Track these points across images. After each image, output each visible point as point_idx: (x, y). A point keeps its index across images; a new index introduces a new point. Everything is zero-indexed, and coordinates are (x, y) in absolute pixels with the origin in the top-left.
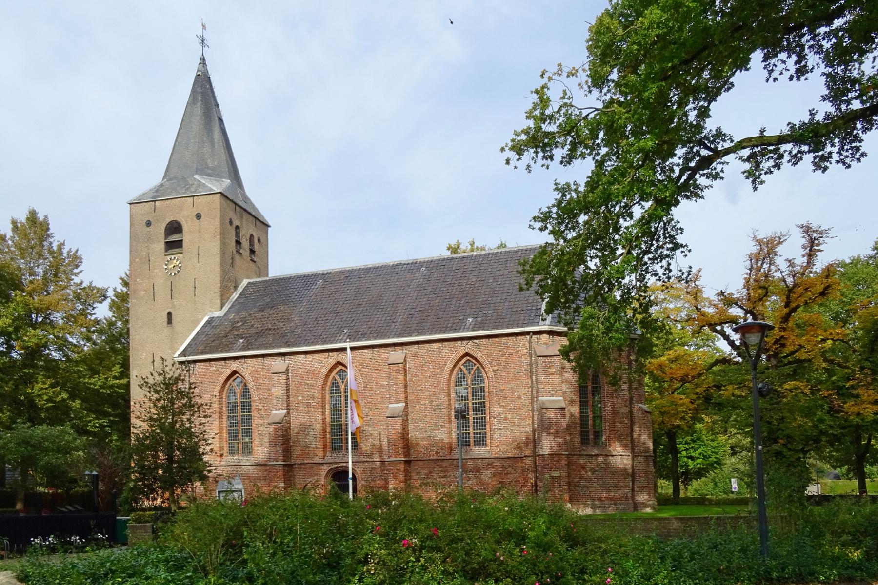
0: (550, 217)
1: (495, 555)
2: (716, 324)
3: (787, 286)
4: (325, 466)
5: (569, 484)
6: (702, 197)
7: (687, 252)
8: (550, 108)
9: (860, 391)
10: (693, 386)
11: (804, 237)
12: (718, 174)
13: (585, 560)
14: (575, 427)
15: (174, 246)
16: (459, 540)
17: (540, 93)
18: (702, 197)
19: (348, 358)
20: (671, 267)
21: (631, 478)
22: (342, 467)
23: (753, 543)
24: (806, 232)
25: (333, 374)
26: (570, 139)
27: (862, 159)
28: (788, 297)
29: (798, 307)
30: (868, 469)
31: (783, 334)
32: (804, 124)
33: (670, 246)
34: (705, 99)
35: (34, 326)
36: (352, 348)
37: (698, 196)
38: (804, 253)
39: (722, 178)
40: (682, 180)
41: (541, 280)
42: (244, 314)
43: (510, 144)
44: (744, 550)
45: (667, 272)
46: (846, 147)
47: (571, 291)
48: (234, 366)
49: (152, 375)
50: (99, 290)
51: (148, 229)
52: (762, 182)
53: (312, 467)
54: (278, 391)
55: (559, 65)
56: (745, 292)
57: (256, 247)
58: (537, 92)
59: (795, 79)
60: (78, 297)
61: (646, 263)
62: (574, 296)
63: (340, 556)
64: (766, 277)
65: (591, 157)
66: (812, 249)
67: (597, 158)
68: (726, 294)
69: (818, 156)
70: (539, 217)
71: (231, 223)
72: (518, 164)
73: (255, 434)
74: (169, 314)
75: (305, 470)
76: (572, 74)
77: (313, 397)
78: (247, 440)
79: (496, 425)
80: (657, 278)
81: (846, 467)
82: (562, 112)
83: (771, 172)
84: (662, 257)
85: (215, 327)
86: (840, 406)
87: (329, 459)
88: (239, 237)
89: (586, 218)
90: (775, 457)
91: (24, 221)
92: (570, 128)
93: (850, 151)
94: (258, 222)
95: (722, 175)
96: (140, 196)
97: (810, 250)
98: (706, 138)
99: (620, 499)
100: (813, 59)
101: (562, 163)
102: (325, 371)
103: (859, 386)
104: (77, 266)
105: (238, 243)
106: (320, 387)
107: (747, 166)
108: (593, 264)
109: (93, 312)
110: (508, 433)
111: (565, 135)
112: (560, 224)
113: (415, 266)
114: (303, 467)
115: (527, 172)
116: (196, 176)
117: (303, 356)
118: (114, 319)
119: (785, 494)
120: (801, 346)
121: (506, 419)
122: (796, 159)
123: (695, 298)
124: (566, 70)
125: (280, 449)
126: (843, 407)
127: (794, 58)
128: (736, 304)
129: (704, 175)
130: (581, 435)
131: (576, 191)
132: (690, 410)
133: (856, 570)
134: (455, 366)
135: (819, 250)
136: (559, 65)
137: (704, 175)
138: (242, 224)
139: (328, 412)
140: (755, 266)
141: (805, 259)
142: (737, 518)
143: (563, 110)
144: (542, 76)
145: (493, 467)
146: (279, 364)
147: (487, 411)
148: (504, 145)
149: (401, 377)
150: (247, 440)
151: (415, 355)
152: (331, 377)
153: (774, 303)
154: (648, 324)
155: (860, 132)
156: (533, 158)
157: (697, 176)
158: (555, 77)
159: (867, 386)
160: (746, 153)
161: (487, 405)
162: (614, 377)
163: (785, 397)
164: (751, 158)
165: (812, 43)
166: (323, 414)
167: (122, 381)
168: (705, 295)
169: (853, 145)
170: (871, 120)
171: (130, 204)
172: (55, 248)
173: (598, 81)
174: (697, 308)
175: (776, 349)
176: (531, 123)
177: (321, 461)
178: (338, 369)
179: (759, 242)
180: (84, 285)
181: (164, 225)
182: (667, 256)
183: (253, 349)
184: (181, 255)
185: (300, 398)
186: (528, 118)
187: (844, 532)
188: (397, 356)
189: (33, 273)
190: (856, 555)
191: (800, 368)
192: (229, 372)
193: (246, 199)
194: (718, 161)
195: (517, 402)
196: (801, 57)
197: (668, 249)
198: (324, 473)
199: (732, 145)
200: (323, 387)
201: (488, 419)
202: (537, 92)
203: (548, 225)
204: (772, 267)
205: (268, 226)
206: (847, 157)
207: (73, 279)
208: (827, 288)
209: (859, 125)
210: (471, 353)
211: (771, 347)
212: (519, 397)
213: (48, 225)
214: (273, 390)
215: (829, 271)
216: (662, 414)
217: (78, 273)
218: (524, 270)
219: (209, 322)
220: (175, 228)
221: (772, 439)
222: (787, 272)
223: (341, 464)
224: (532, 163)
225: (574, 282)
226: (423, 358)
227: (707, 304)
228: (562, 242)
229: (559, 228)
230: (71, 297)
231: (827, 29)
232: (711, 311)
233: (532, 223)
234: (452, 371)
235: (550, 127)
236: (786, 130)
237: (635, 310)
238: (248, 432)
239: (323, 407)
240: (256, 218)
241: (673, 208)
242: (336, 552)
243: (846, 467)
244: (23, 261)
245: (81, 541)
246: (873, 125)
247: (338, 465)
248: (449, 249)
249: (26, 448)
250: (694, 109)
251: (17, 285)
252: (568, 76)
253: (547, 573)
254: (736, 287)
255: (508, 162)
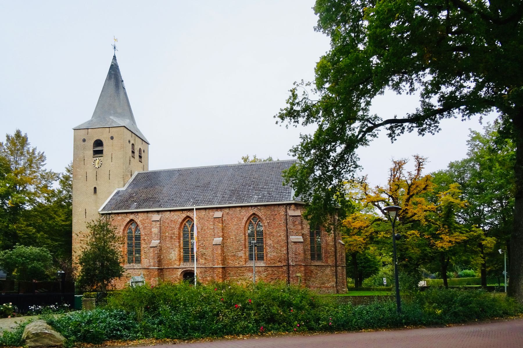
0: (298, 150)
1: (278, 312)
2: (375, 202)
3: (408, 185)
4: (180, 270)
5: (305, 280)
6: (369, 145)
7: (361, 169)
8: (298, 99)
9: (442, 236)
10: (364, 232)
11: (415, 161)
12: (376, 135)
13: (319, 315)
14: (308, 251)
15: (98, 153)
16: (261, 305)
17: (293, 91)
18: (369, 145)
19: (194, 215)
20: (354, 176)
21: (335, 277)
22: (189, 270)
23: (394, 307)
24: (417, 159)
25: (185, 222)
26: (306, 114)
27: (439, 131)
28: (409, 190)
29: (413, 195)
30: (448, 273)
31: (406, 207)
32: (414, 114)
33: (354, 166)
34: (369, 97)
35: (18, 192)
36: (196, 209)
37: (366, 144)
38: (416, 169)
39: (377, 137)
40: (359, 137)
41: (293, 180)
42: (136, 189)
43: (278, 115)
44: (390, 310)
45: (352, 178)
46: (432, 125)
47: (307, 186)
48: (132, 217)
49: (93, 221)
50: (55, 174)
51: (84, 143)
52: (395, 140)
53: (173, 270)
54: (155, 230)
55: (302, 80)
56: (389, 186)
57: (143, 155)
58: (291, 91)
59: (409, 94)
60: (43, 177)
61: (342, 174)
62: (309, 188)
63: (205, 312)
64: (398, 179)
65: (317, 122)
66: (419, 166)
67: (319, 123)
68: (379, 187)
69: (420, 129)
70: (292, 150)
71: (129, 142)
72: (282, 124)
73: (142, 252)
74: (95, 188)
75: (169, 271)
76: (308, 84)
77: (174, 234)
78: (137, 255)
79: (269, 250)
80: (347, 181)
81: (438, 273)
82: (303, 102)
83: (399, 135)
84: (350, 171)
85: (120, 196)
86: (433, 243)
87: (182, 266)
88: (134, 149)
89: (315, 151)
90: (404, 267)
91: (13, 136)
92: (307, 108)
93: (434, 127)
94: (143, 142)
95: (377, 135)
96: (79, 126)
97: (419, 168)
98: (370, 118)
99: (330, 288)
100: (416, 85)
101: (302, 124)
102: (180, 220)
103: (442, 234)
104: (43, 161)
105: (133, 152)
106: (178, 229)
107: (389, 132)
108: (318, 173)
109: (52, 186)
110: (275, 254)
111: (304, 112)
112: (302, 154)
113: (226, 168)
114: (168, 270)
115: (286, 128)
116: (111, 117)
117: (169, 213)
118: (61, 189)
119: (407, 285)
120: (415, 214)
121: (274, 247)
122: (411, 130)
123: (365, 188)
124: (305, 83)
125: (156, 260)
126: (435, 243)
127: (409, 84)
128: (384, 192)
129: (369, 135)
130: (311, 256)
131: (310, 138)
132: (363, 243)
133: (439, 319)
134: (248, 220)
135: (423, 168)
136: (302, 80)
137: (369, 135)
138: (135, 142)
139: (182, 242)
140: (393, 174)
141: (416, 172)
142: (386, 296)
143: (304, 100)
144: (294, 84)
145: (267, 271)
146: (156, 217)
147: (264, 243)
148: (275, 115)
149: (220, 225)
150: (137, 255)
151: (228, 214)
152: (184, 224)
153: (402, 192)
154: (343, 202)
155: (438, 119)
156: (289, 122)
157: (366, 135)
158: (300, 85)
159: (446, 234)
160: (388, 126)
161: (264, 239)
162: (328, 228)
163: (408, 238)
164: (391, 128)
165: (416, 78)
166: (179, 242)
167: (67, 223)
168: (369, 187)
169: (435, 125)
170: (443, 114)
171: (74, 130)
172: (31, 151)
173: (320, 86)
174: (366, 194)
175: (404, 214)
176: (289, 106)
177: (178, 267)
178: (187, 220)
179: (395, 162)
180: (46, 172)
181: (93, 142)
182: (353, 171)
183: (142, 208)
184: (102, 158)
185: (167, 234)
186: (287, 103)
187: (434, 302)
188: (218, 214)
189: (17, 163)
190: (439, 312)
191: (416, 225)
192: (128, 220)
193: (138, 130)
194: (376, 129)
195: (280, 238)
196: (412, 84)
197: (353, 167)
198: (179, 273)
199: (382, 122)
200: (179, 229)
201: (264, 247)
202: (291, 91)
203: (297, 154)
204: (401, 175)
205: (148, 144)
206: (433, 130)
207: (40, 168)
208: (427, 186)
209: (438, 116)
210: (256, 213)
211: (401, 213)
212: (280, 236)
213: (27, 138)
214: (153, 230)
215: (427, 178)
216: (350, 245)
217: (44, 165)
218: (285, 175)
219: (118, 193)
220: (99, 143)
221: (402, 258)
222: (408, 178)
223: (189, 269)
224: (289, 124)
225: (309, 182)
226: (232, 215)
227: (371, 191)
228: (303, 162)
229: (302, 155)
230: (39, 177)
231: (423, 73)
232: (372, 195)
233: (289, 152)
234: (246, 222)
235: (297, 108)
236: (406, 117)
237: (338, 196)
238: (139, 252)
239: (179, 239)
240: (142, 140)
241: (355, 149)
242: (203, 310)
243: (438, 273)
244: (13, 157)
245: (56, 308)
246: (443, 116)
247: (187, 269)
248: (242, 159)
249: (21, 259)
250: (364, 102)
251: (8, 170)
252: (306, 85)
253: (302, 320)
254: (385, 184)
255: (277, 123)
